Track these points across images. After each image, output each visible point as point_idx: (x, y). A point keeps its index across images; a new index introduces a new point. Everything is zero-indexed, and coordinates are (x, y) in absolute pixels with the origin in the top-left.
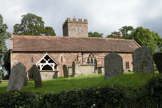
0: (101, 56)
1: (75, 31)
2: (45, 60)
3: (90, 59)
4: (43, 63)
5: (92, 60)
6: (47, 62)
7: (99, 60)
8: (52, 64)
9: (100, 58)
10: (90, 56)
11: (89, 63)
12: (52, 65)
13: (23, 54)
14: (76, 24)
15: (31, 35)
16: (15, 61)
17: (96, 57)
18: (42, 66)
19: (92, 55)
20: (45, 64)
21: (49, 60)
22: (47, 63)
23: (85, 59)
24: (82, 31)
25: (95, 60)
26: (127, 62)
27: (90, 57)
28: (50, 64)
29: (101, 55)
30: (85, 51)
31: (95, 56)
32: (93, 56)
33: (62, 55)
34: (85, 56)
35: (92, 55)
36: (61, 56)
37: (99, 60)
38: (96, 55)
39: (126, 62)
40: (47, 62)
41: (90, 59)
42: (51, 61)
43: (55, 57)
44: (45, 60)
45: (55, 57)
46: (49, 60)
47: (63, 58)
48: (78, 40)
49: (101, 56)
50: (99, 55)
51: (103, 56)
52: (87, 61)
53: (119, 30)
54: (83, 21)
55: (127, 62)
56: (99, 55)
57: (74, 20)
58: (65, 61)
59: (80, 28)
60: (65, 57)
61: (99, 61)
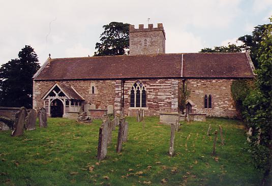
0: (154, 86)
1: (141, 45)
2: (55, 92)
3: (135, 90)
5: (138, 91)
7: (150, 92)
9: (151, 89)
10: (135, 85)
11: (62, 92)
13: (105, 78)
14: (144, 33)
16: (37, 93)
17: (146, 86)
18: (51, 100)
20: (54, 98)
21: (59, 92)
22: (57, 97)
23: (126, 90)
24: (152, 44)
25: (144, 91)
26: (208, 96)
27: (135, 87)
28: (60, 98)
29: (154, 84)
31: (144, 85)
33: (93, 84)
34: (127, 86)
36: (92, 86)
38: (145, 83)
39: (206, 96)
41: (135, 90)
44: (55, 92)
46: (59, 92)
47: (95, 88)
48: (143, 58)
49: (154, 86)
50: (151, 84)
52: (130, 93)
53: (242, 39)
54: (155, 26)
55: (208, 96)
57: (151, 26)
58: (97, 93)
59: (148, 39)
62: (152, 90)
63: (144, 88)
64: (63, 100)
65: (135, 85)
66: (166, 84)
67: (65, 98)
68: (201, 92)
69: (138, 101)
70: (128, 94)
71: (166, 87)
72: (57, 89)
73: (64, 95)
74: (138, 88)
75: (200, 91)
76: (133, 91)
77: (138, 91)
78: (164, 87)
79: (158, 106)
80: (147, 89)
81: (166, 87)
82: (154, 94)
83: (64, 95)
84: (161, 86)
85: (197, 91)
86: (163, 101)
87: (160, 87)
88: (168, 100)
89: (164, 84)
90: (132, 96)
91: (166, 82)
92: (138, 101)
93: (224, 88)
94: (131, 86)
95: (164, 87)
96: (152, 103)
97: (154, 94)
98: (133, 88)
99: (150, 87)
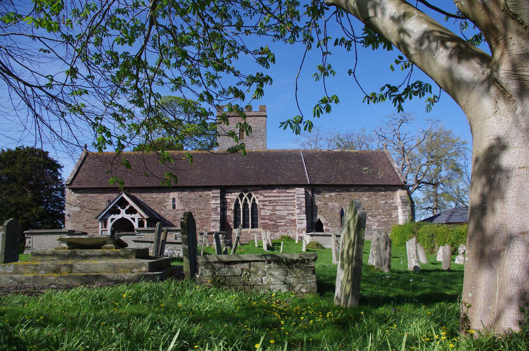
0: (271, 197)
4: (131, 214)
5: (245, 205)
6: (123, 211)
8: (133, 216)
10: (241, 196)
11: (131, 207)
12: (112, 219)
15: (505, 89)
17: (257, 197)
19: (245, 195)
20: (117, 217)
21: (127, 207)
25: (254, 205)
28: (128, 217)
29: (270, 194)
30: (230, 183)
31: (254, 196)
32: (250, 196)
33: (173, 195)
35: (245, 195)
37: (263, 205)
40: (123, 211)
42: (132, 211)
43: (158, 200)
45: (158, 200)
46: (127, 207)
49: (271, 197)
50: (266, 194)
51: (275, 194)
56: (266, 194)
58: (181, 208)
60: (181, 198)
61: (265, 207)
62: (267, 203)
63: (254, 200)
64: (133, 219)
65: (241, 196)
66: (287, 194)
67: (136, 216)
68: (337, 205)
69: (246, 219)
70: (231, 209)
71: (288, 198)
72: (123, 203)
73: (135, 212)
74: (246, 200)
75: (334, 204)
76: (237, 205)
77: (245, 205)
78: (285, 198)
79: (277, 227)
80: (259, 201)
81: (288, 198)
82: (271, 208)
83: (135, 212)
84: (280, 197)
85: (330, 204)
86: (284, 219)
87: (278, 198)
88: (290, 217)
89: (284, 194)
90: (236, 211)
91: (288, 191)
92: (246, 219)
93: (366, 199)
94: (235, 198)
95: (285, 198)
96: (268, 221)
97: (271, 208)
98: (237, 200)
99: (264, 199)
